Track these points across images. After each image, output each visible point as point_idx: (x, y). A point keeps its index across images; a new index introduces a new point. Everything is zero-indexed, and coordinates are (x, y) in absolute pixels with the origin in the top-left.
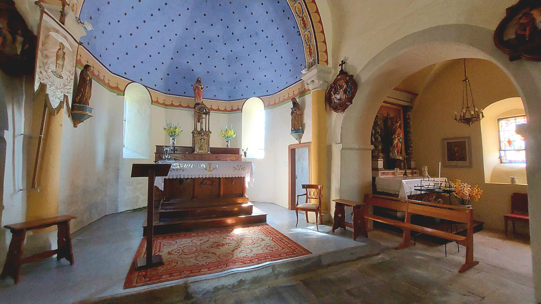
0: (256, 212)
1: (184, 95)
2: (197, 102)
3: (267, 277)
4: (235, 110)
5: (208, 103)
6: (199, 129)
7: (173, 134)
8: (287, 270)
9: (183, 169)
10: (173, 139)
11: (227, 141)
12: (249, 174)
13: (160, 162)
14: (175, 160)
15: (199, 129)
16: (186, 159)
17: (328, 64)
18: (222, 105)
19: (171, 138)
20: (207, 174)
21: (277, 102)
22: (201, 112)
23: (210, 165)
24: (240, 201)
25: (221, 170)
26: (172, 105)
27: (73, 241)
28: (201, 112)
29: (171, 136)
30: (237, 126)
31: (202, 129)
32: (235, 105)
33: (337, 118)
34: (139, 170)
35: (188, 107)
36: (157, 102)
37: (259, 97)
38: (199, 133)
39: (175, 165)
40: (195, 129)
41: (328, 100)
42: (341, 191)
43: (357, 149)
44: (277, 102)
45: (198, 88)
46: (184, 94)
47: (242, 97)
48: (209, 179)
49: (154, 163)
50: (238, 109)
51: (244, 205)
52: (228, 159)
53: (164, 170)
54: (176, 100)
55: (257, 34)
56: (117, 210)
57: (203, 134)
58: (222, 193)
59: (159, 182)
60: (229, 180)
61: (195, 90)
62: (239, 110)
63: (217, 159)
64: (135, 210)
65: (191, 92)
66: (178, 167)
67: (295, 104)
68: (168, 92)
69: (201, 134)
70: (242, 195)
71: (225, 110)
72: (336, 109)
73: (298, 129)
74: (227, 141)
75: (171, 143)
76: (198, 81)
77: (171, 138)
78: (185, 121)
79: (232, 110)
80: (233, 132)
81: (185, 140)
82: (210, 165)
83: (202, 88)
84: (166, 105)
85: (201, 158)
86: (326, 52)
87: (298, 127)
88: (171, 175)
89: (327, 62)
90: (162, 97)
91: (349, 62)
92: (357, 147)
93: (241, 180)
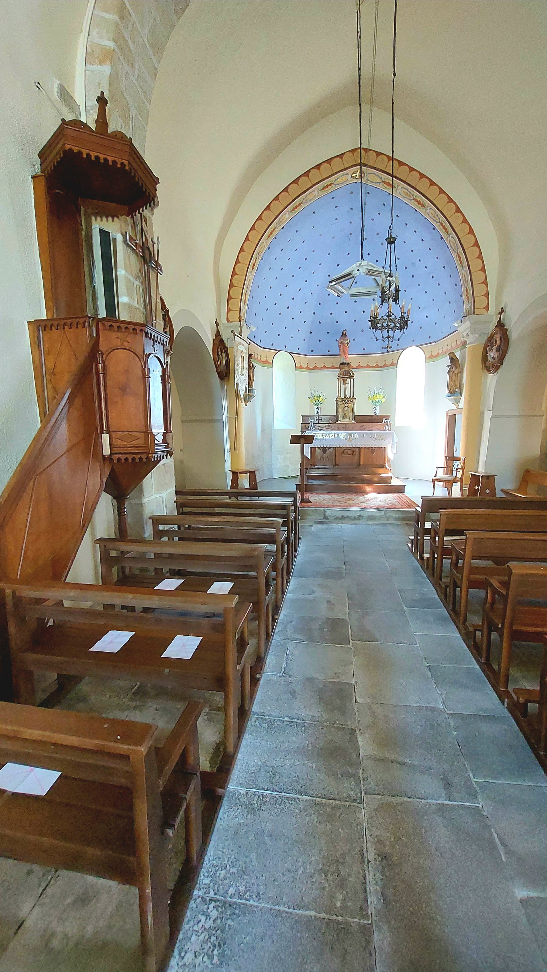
0: (395, 482)
1: (329, 353)
2: (342, 361)
3: (380, 518)
4: (389, 365)
5: (353, 360)
6: (343, 396)
7: (317, 404)
8: (397, 516)
9: (325, 438)
10: (318, 408)
11: (375, 407)
12: (391, 445)
13: (306, 433)
14: (320, 430)
15: (343, 396)
16: (330, 428)
17: (488, 310)
18: (372, 360)
19: (316, 407)
20: (348, 444)
21: (440, 352)
22: (346, 373)
23: (350, 434)
24: (380, 471)
25: (360, 439)
26: (316, 368)
27: (258, 484)
28: (346, 373)
29: (315, 405)
30: (390, 388)
31: (346, 396)
32: (389, 357)
33: (491, 379)
34: (295, 439)
35: (333, 367)
36: (301, 367)
37: (418, 346)
38: (343, 401)
39: (319, 435)
40: (339, 396)
41: (485, 358)
42: (486, 463)
43: (516, 416)
44: (440, 352)
45: (343, 344)
46: (329, 353)
47: (398, 348)
48: (349, 448)
49: (300, 434)
50: (392, 364)
51: (381, 475)
52: (374, 428)
53: (309, 439)
54: (319, 361)
55: (414, 265)
56: (272, 476)
57: (346, 401)
58: (361, 463)
59: (307, 447)
60: (372, 450)
61: (340, 347)
62: (395, 365)
63: (362, 429)
64: (285, 478)
65: (335, 349)
66: (322, 437)
67: (453, 360)
68: (312, 353)
69: (345, 401)
70: (382, 466)
71: (377, 366)
72: (488, 370)
73: (455, 392)
74: (375, 407)
75: (316, 412)
76: (344, 335)
77: (316, 407)
78: (328, 384)
79: (385, 365)
80: (382, 396)
81: (329, 408)
82: (350, 434)
83: (348, 344)
84: (311, 369)
85: (345, 428)
86: (487, 295)
87: (454, 391)
88: (314, 444)
89: (487, 308)
90: (304, 360)
91: (508, 310)
92: (518, 414)
93: (383, 450)
